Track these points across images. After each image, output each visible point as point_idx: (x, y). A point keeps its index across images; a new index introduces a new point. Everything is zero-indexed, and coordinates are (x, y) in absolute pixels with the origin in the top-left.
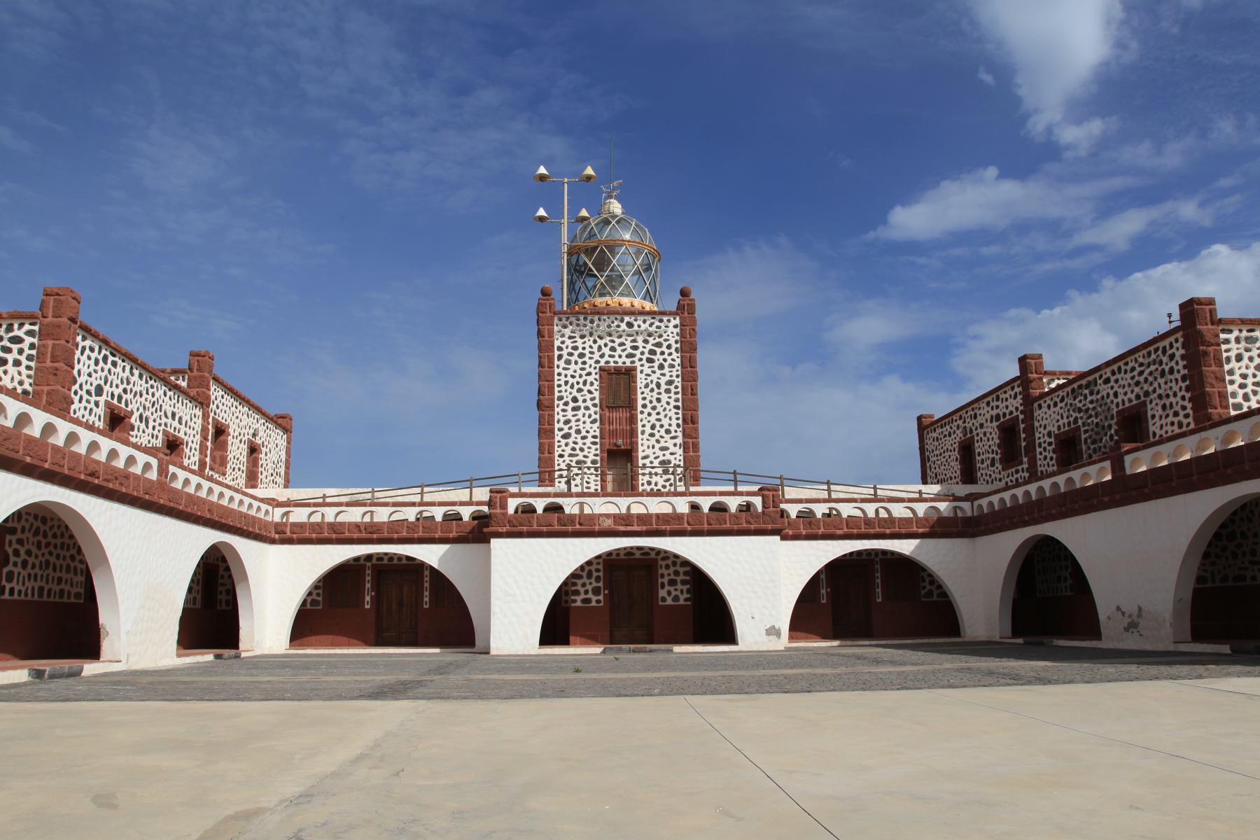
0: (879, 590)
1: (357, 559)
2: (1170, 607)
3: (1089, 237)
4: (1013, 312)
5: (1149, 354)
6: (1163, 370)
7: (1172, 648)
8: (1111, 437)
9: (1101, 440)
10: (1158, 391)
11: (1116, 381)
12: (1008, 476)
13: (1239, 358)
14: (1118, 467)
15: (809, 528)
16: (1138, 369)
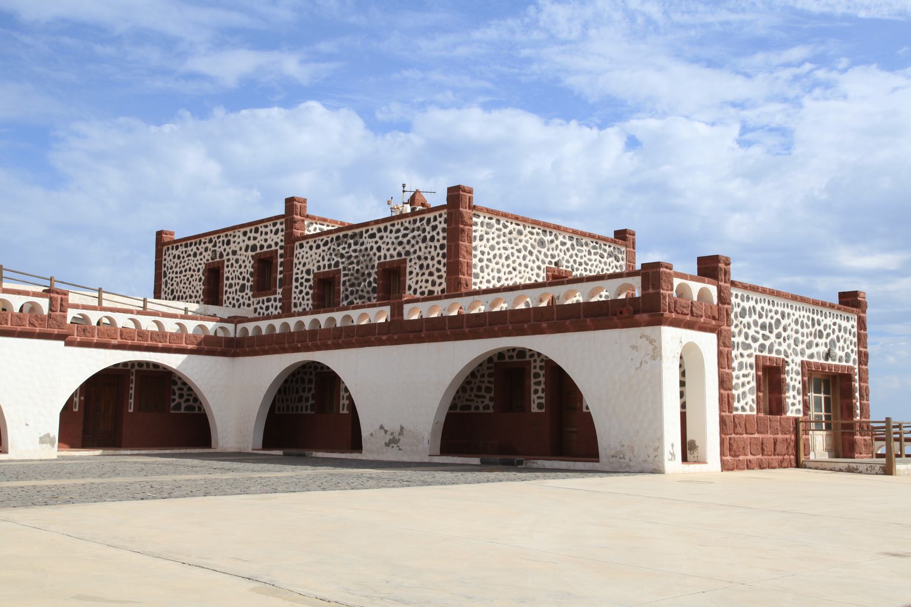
0: (132, 401)
1: (125, 364)
2: (429, 428)
3: (200, 64)
4: (122, 120)
5: (415, 221)
6: (425, 237)
7: (427, 460)
8: (370, 283)
9: (359, 285)
10: (418, 253)
11: (381, 238)
12: (258, 304)
13: (481, 239)
14: (397, 311)
15: (82, 336)
16: (403, 232)
